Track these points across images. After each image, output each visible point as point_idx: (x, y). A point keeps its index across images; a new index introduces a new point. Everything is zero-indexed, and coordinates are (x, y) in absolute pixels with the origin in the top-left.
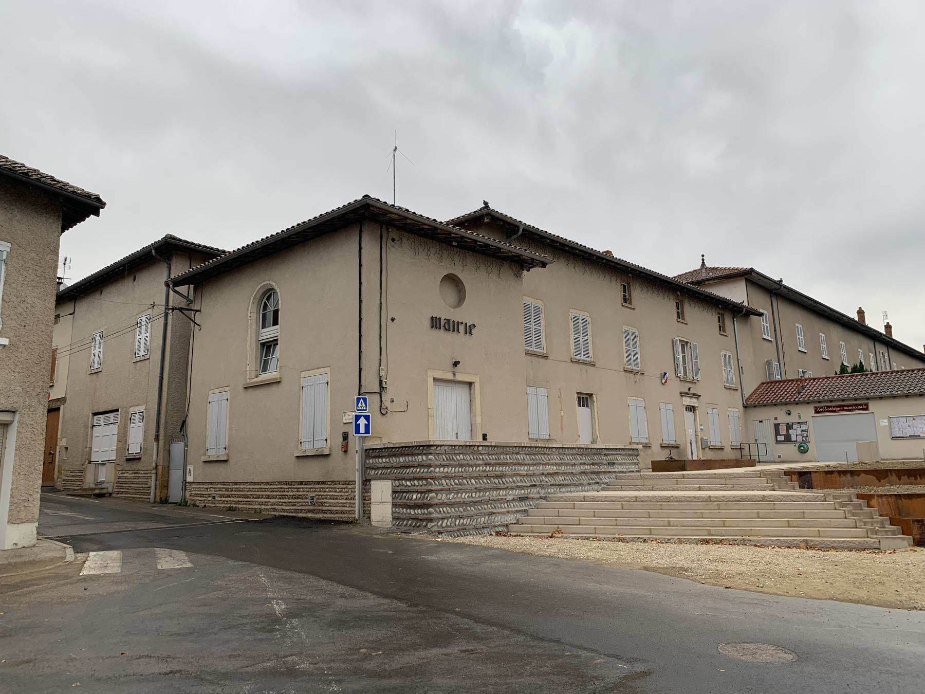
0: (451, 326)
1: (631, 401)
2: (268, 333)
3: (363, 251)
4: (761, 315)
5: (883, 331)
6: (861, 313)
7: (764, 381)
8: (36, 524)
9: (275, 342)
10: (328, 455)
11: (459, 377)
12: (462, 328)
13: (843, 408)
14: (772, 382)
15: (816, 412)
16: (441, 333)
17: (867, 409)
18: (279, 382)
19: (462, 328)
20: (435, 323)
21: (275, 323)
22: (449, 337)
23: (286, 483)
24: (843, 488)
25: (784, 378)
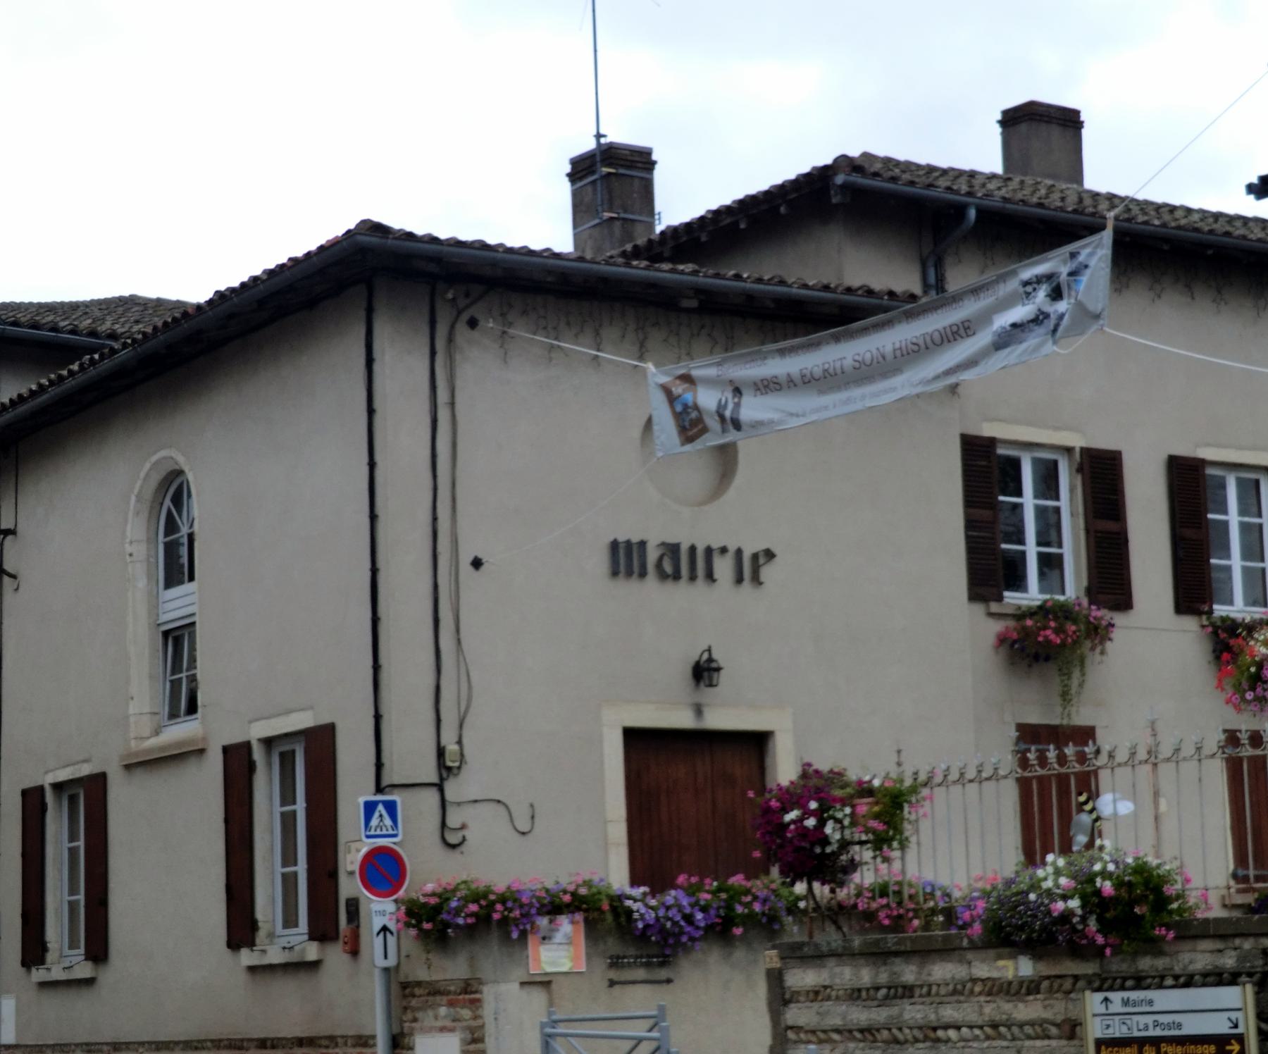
0: (682, 564)
3: (377, 367)
8: (1088, 993)
9: (957, 385)
12: (724, 568)
16: (650, 592)
19: (724, 568)
20: (626, 559)
21: (191, 578)
22: (683, 596)
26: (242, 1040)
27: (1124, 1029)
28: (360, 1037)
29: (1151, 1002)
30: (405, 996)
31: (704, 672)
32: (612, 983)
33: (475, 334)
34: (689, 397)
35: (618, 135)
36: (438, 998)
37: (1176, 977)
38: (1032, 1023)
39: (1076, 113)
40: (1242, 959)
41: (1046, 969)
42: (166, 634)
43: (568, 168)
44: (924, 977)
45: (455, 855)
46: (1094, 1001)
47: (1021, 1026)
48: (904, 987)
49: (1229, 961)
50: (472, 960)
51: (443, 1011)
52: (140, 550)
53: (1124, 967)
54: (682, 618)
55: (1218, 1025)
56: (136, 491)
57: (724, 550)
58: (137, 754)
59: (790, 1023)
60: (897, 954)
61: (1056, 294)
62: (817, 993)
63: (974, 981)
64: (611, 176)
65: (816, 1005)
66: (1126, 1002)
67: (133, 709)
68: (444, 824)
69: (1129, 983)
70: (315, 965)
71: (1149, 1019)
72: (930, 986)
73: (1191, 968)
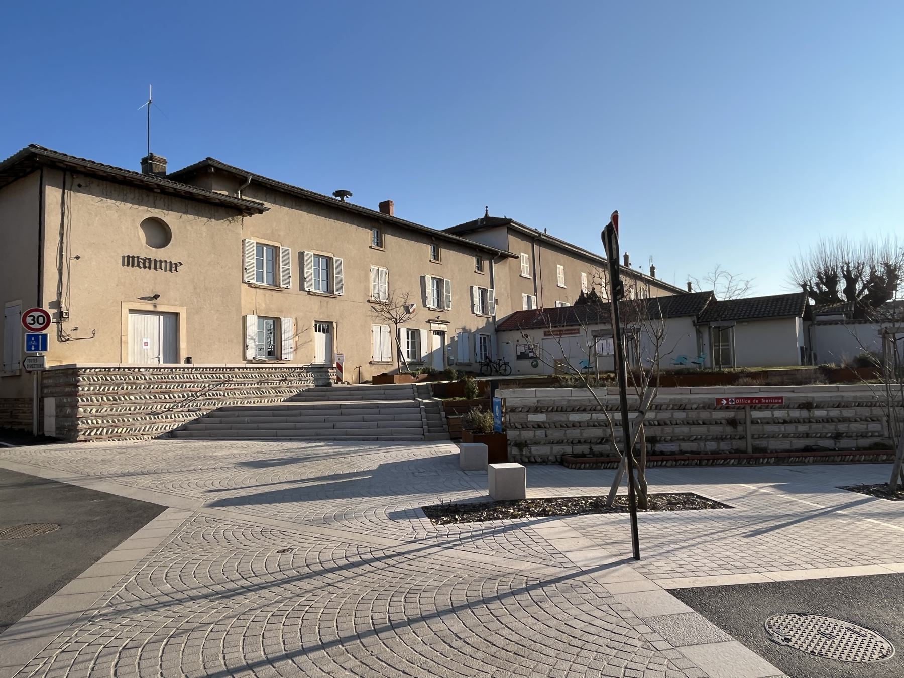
0: (148, 264)
1: (375, 328)
10: (19, 376)
11: (160, 309)
15: (545, 335)
17: (578, 333)
20: (130, 261)
24: (674, 385)
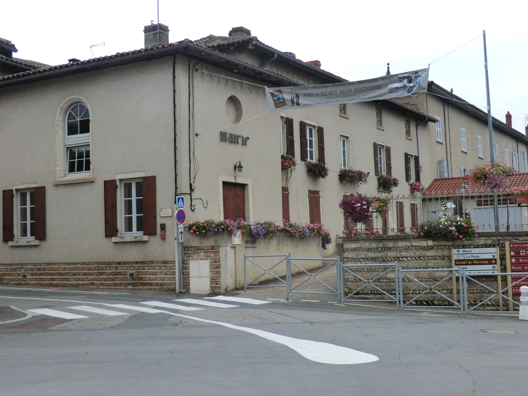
2: (78, 139)
3: (176, 79)
4: (434, 121)
5: (504, 120)
6: (509, 117)
7: (436, 178)
13: (65, 75)
14: (443, 180)
15: (478, 205)
16: (227, 146)
18: (93, 182)
23: (104, 263)
25: (450, 177)
26: (110, 262)
27: (463, 258)
28: (165, 261)
29: (471, 251)
30: (185, 250)
31: (238, 167)
32: (246, 248)
33: (197, 73)
34: (281, 96)
35: (163, 22)
36: (199, 251)
37: (474, 246)
38: (432, 256)
39: (167, 27)
40: (492, 242)
41: (436, 243)
42: (67, 148)
43: (144, 29)
44: (396, 245)
45: (193, 212)
46: (455, 251)
47: (428, 257)
48: (388, 248)
49: (489, 242)
50: (216, 241)
51: (202, 254)
52: (61, 124)
53: (460, 243)
54: (234, 153)
55: (490, 257)
56: (60, 107)
57: (240, 136)
58: (59, 182)
59: (345, 257)
60: (386, 240)
61: (410, 81)
62: (355, 249)
63: (412, 246)
64: (157, 31)
65: (355, 252)
66: (464, 251)
67: (57, 169)
68: (191, 205)
69: (461, 247)
70: (145, 242)
71: (470, 255)
72: (397, 248)
73: (479, 244)
